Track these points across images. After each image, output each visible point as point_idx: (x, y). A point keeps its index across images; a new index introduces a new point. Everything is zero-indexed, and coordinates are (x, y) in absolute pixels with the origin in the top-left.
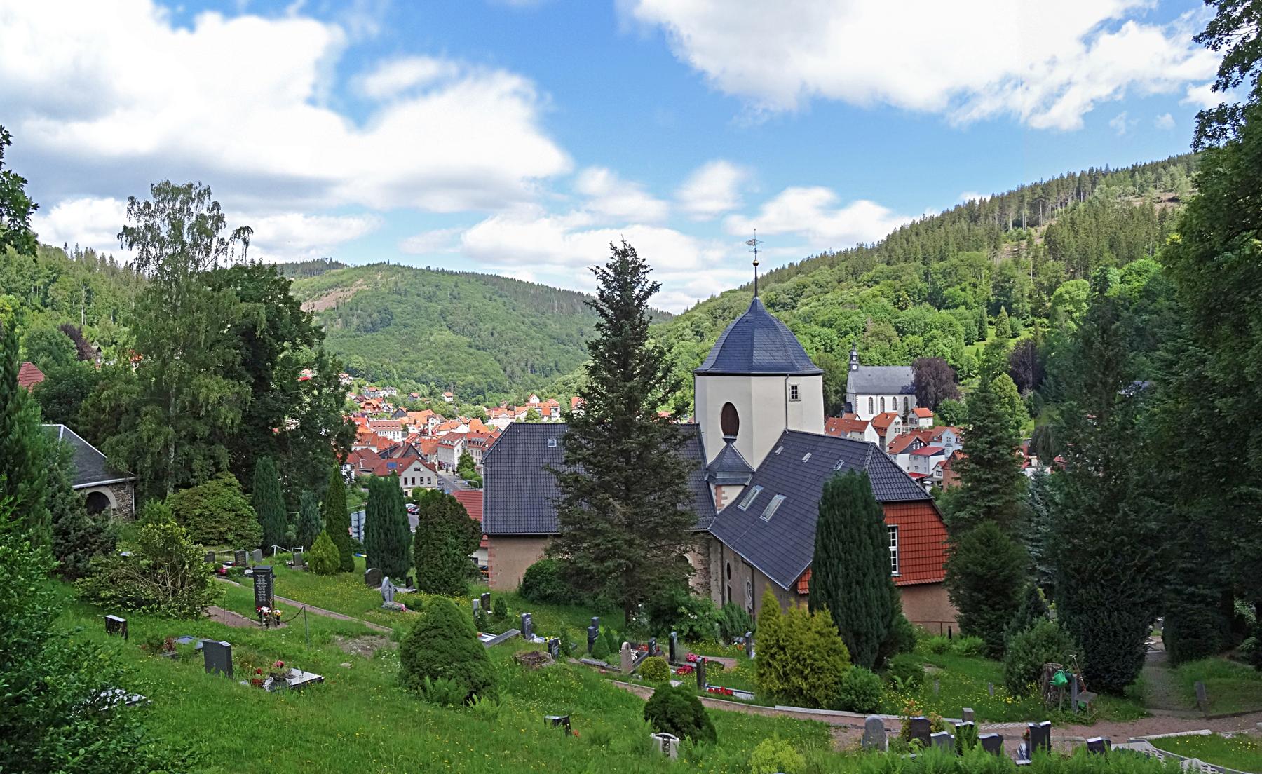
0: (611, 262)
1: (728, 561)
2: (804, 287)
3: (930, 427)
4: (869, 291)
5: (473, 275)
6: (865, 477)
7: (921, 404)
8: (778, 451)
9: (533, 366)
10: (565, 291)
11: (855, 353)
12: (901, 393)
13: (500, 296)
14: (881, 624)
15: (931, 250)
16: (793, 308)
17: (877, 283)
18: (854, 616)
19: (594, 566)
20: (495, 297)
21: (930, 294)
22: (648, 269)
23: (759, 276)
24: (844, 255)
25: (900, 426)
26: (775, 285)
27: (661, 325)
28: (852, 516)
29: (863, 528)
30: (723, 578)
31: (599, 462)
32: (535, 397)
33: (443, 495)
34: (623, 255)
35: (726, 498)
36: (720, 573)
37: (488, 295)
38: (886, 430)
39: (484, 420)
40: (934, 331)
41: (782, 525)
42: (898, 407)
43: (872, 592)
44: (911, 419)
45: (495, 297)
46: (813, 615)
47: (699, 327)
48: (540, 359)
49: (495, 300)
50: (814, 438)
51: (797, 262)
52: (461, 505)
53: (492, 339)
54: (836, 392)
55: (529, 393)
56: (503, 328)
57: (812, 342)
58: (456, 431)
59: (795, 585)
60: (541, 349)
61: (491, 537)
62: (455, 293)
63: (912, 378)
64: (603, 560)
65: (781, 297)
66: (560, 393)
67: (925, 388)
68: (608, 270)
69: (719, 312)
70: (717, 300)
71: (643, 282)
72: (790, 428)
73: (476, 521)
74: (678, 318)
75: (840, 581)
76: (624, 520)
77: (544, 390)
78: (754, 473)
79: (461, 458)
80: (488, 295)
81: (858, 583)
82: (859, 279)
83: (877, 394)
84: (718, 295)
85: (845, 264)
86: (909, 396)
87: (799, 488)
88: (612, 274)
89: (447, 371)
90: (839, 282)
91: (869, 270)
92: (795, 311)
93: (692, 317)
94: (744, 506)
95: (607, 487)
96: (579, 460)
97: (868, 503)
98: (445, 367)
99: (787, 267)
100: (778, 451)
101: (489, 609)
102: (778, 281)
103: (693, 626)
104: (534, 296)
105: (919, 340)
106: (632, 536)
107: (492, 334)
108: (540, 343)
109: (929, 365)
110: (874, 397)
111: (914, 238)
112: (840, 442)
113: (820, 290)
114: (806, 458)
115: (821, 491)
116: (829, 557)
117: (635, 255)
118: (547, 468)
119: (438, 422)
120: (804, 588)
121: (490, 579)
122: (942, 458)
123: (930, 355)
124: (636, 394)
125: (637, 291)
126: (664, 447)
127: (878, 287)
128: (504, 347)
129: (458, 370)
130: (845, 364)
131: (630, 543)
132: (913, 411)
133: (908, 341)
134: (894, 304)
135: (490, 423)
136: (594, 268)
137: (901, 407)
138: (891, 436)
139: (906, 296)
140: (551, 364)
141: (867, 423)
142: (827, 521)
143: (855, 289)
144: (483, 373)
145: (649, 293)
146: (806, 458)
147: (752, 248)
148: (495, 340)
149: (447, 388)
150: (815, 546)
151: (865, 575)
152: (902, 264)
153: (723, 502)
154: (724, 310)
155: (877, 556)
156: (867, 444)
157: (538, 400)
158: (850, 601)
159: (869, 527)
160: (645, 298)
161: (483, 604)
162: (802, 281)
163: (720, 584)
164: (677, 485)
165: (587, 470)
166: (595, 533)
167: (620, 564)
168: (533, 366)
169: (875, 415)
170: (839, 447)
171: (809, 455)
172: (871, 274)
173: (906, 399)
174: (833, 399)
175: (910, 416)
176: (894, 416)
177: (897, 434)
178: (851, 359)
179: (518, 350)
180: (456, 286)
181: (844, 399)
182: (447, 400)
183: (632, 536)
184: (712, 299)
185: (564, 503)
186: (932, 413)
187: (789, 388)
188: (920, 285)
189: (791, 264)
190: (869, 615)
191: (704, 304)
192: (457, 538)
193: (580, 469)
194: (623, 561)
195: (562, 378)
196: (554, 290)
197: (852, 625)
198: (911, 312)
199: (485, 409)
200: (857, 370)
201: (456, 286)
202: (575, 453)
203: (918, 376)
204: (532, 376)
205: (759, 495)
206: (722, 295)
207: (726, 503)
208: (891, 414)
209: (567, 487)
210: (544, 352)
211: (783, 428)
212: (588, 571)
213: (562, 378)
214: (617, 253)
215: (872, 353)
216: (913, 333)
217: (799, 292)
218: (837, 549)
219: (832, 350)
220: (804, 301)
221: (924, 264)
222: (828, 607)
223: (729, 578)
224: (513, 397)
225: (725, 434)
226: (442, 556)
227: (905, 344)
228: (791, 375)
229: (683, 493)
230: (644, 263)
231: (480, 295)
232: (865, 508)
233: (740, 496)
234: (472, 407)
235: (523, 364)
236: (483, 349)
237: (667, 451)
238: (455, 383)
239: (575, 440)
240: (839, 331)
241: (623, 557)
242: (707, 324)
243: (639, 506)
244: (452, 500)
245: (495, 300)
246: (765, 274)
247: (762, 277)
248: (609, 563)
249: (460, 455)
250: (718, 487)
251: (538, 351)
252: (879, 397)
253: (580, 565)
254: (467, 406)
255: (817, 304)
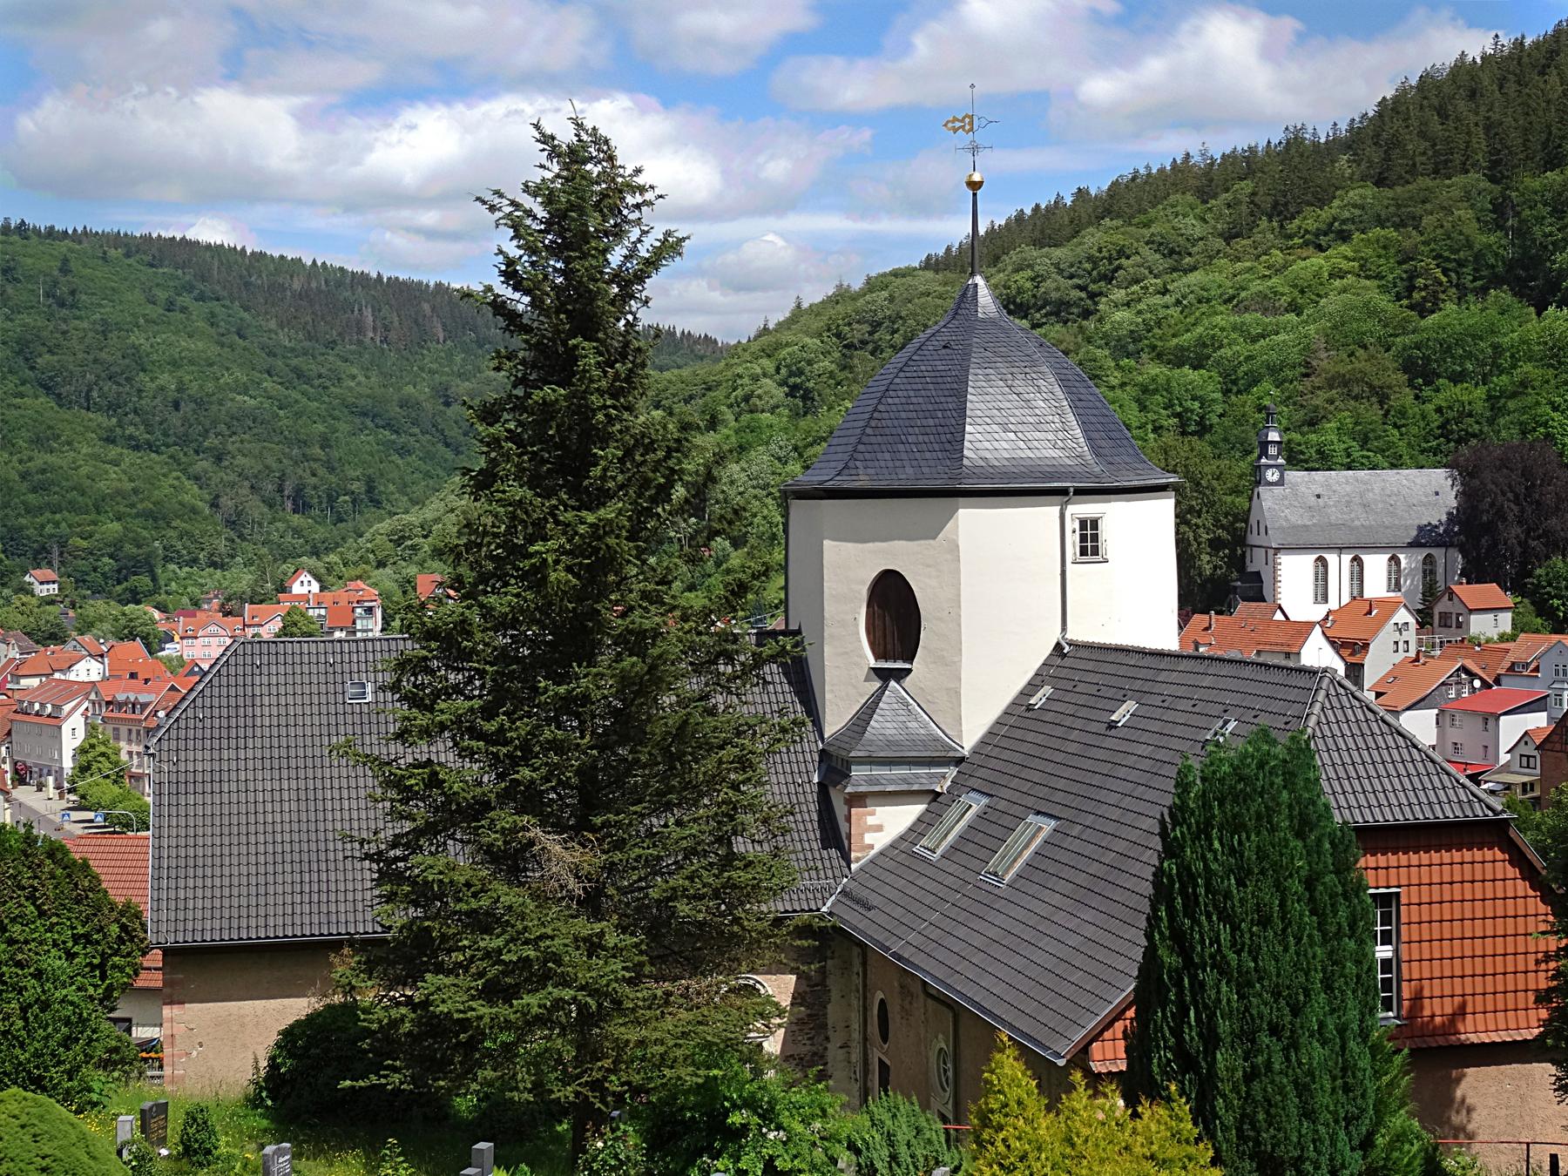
0: (537, 176)
1: (880, 995)
2: (1122, 253)
3: (1503, 638)
4: (1317, 260)
5: (117, 240)
6: (1302, 752)
7: (1474, 574)
8: (1037, 700)
9: (299, 492)
10: (394, 283)
11: (1274, 436)
12: (1415, 544)
13: (201, 298)
14: (1342, 1134)
15: (1515, 139)
16: (1086, 314)
17: (1344, 237)
18: (1261, 1116)
19: (483, 1009)
20: (185, 300)
21: (1511, 265)
22: (649, 196)
23: (982, 231)
24: (1244, 165)
25: (1411, 635)
26: (1032, 253)
27: (685, 372)
28: (1261, 854)
29: (1296, 886)
30: (865, 1039)
31: (501, 729)
32: (306, 577)
33: (29, 839)
34: (573, 158)
35: (879, 828)
36: (856, 1026)
37: (162, 295)
38: (1366, 646)
39: (153, 642)
40: (1527, 367)
41: (1047, 895)
42: (1406, 584)
43: (1317, 1053)
44: (1445, 616)
45: (185, 300)
46: (1135, 1115)
47: (800, 372)
48: (321, 472)
49: (184, 310)
50: (1148, 661)
51: (1098, 185)
52: (85, 866)
53: (175, 419)
54: (1216, 545)
55: (288, 567)
56: (210, 387)
57: (1143, 408)
58: (72, 676)
59: (1083, 1052)
60: (325, 443)
61: (176, 956)
62: (61, 291)
63: (1450, 500)
64: (508, 994)
65: (1049, 284)
66: (381, 564)
67: (1489, 528)
68: (528, 202)
69: (860, 332)
70: (854, 297)
71: (635, 233)
72: (1068, 636)
73: (128, 905)
74: (735, 351)
75: (1224, 1027)
76: (572, 883)
77: (333, 558)
78: (960, 761)
79: (81, 751)
80: (162, 295)
81: (1275, 1030)
82: (1292, 226)
83: (1340, 549)
84: (857, 284)
85: (1247, 186)
86: (1438, 553)
87: (1102, 795)
88: (541, 213)
89: (40, 510)
90: (1229, 237)
91: (1322, 202)
92: (1090, 324)
93: (779, 346)
94: (938, 844)
95: (529, 800)
96: (443, 727)
97: (1308, 818)
98: (32, 498)
99: (1068, 201)
100: (1037, 700)
101: (162, 1142)
102: (1038, 243)
103: (772, 1158)
104: (304, 295)
105: (1474, 395)
106: (597, 927)
107: (176, 406)
108: (320, 427)
109: (1504, 464)
110: (1332, 558)
111: (1462, 105)
112: (1226, 670)
113: (1169, 263)
114: (1122, 714)
115: (1170, 785)
116: (1189, 964)
117: (611, 158)
118: (345, 750)
119: (14, 653)
120: (1110, 1056)
121: (167, 1071)
122: (1538, 721)
123: (1509, 434)
124: (611, 541)
125: (616, 257)
126: (693, 685)
127: (1345, 249)
128: (211, 441)
129: (73, 507)
130: (1244, 466)
131: (593, 946)
132: (1452, 594)
133: (1440, 400)
134: (1398, 298)
135: (170, 650)
136: (488, 197)
137: (1412, 583)
138: (1377, 663)
139: (1438, 273)
140: (355, 486)
141: (1310, 626)
142: (1184, 868)
143: (1277, 256)
144: (147, 515)
145: (652, 263)
146: (1122, 714)
147: (963, 138)
148: (185, 420)
149: (40, 557)
150: (1149, 936)
151: (1296, 1011)
152: (1427, 182)
153: (869, 838)
154: (876, 326)
155: (1334, 959)
156: (1311, 672)
157: (315, 587)
158: (1249, 1078)
159: (1309, 884)
160: (640, 277)
161: (144, 1128)
162: (1119, 238)
163: (856, 1056)
164: (735, 787)
165: (466, 753)
166: (483, 922)
167: (559, 1004)
168: (299, 492)
169: (1333, 604)
170: (1222, 683)
171: (1130, 706)
172: (1326, 214)
173: (1429, 560)
174: (1206, 562)
175: (1442, 606)
176: (1389, 607)
177: (1401, 655)
178: (1264, 453)
179: (256, 447)
180: (65, 270)
181: (1238, 563)
182: (43, 591)
183: (597, 927)
184: (841, 296)
185: (394, 846)
186: (1509, 600)
187: (1072, 525)
188: (1481, 239)
189: (1081, 194)
190: (1308, 1114)
191: (815, 310)
192: (71, 956)
193: (442, 752)
194: (567, 994)
195: (385, 526)
196: (361, 279)
197: (1257, 1143)
198: (1451, 315)
199: (157, 615)
200: (1280, 482)
201: (65, 270)
202: (431, 709)
203: (1469, 496)
204: (296, 519)
205: (980, 817)
206: (872, 285)
207: (878, 841)
208: (1381, 601)
209: (405, 801)
210: (335, 454)
211: (1054, 636)
212: (464, 1024)
213: (385, 526)
214: (554, 153)
215: (1328, 434)
216: (1456, 378)
217: (1104, 267)
218: (1218, 941)
219: (1203, 429)
220: (1119, 295)
221: (1493, 179)
222: (1182, 1093)
223: (885, 1039)
224: (243, 579)
225: (877, 658)
226: (24, 1009)
227: (1430, 407)
228: (1080, 492)
229: (751, 808)
230: (640, 180)
231: (138, 296)
232: (1300, 835)
233: (919, 820)
234: (115, 609)
235: (269, 487)
236: (151, 447)
237: (704, 697)
238: (63, 545)
239: (432, 672)
240: (1225, 375)
241: (565, 983)
242: (826, 364)
243: (619, 845)
244: (55, 852)
245: (184, 310)
246: (1001, 221)
247: (991, 232)
248: (532, 1001)
249: (77, 743)
250: (858, 800)
251: (317, 451)
252: (1347, 558)
253: (443, 1008)
254: (98, 606)
255: (1158, 300)
